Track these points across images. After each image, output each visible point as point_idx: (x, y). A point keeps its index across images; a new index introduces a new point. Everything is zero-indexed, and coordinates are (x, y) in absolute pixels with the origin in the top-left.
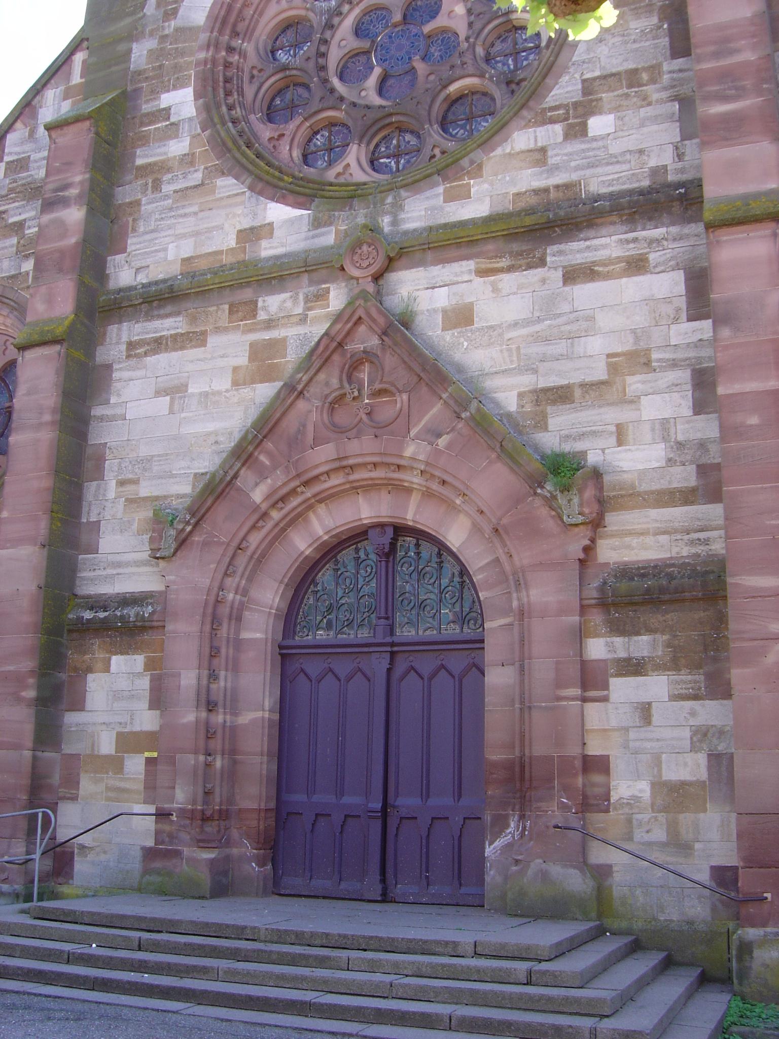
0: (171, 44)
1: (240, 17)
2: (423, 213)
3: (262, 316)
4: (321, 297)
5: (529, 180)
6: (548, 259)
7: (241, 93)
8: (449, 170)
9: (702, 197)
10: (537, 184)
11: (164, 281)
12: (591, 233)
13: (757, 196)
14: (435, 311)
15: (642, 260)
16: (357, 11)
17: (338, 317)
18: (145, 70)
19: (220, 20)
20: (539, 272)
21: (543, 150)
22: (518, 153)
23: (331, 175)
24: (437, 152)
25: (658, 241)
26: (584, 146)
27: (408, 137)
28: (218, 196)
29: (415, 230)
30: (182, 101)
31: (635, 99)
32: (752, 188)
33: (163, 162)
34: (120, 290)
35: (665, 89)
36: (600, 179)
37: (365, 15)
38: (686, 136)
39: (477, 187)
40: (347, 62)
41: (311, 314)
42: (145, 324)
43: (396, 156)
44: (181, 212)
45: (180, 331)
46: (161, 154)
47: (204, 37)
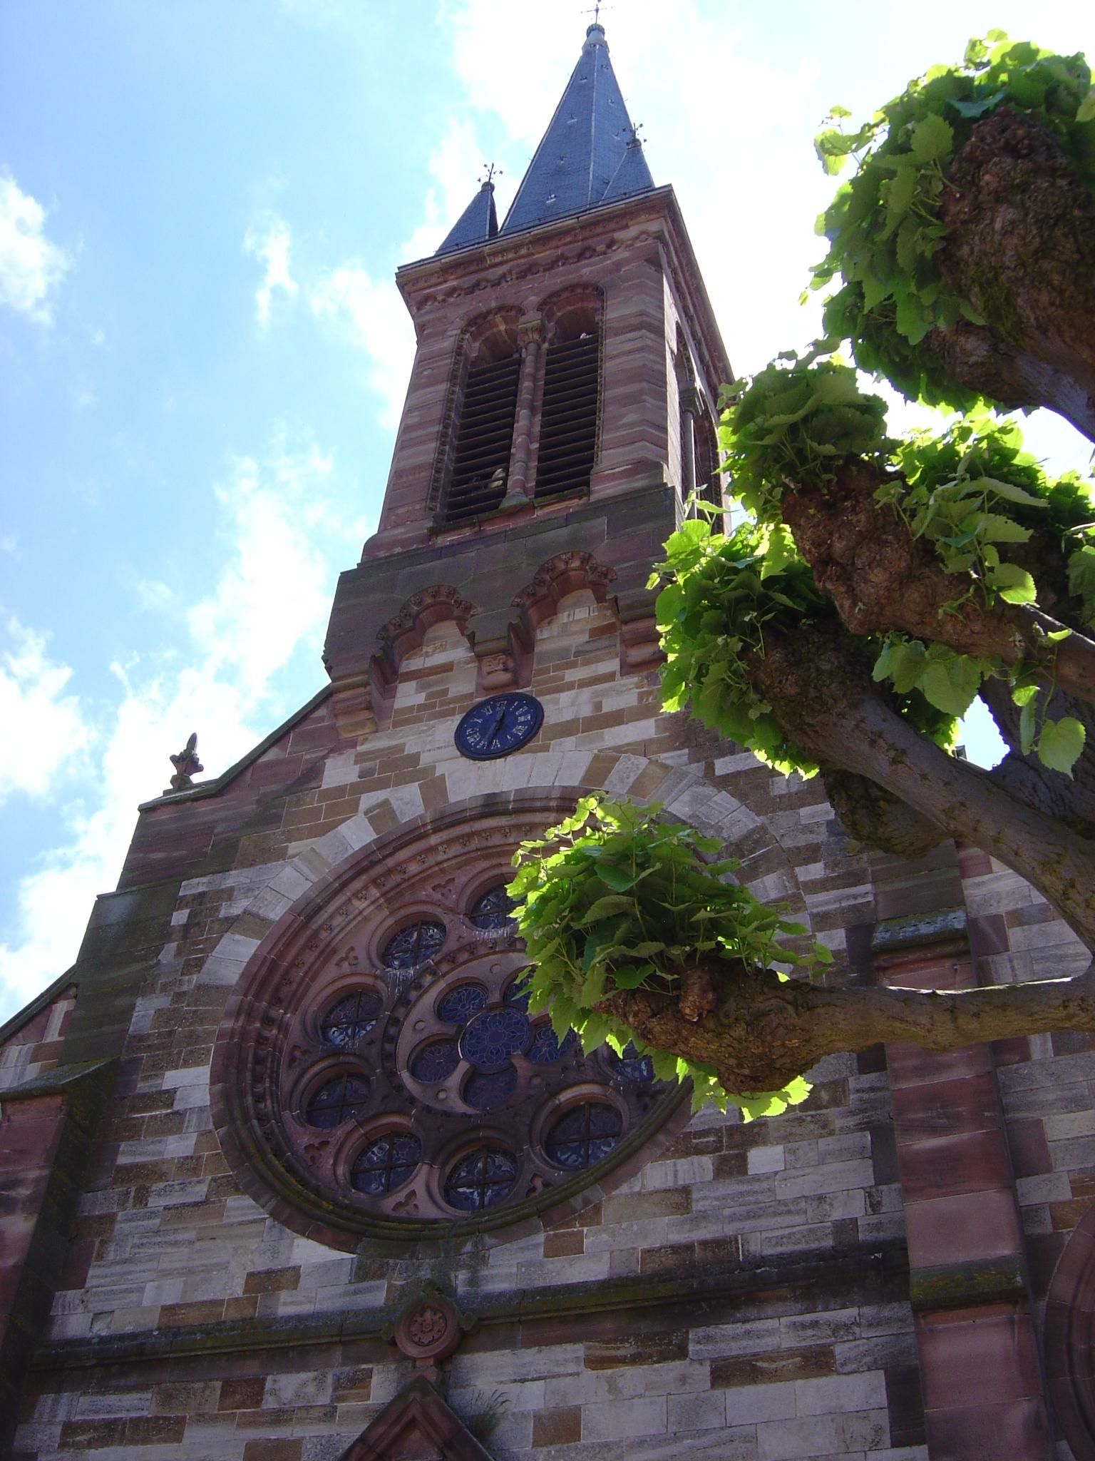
0: (188, 1005)
1: (286, 979)
2: (515, 1270)
3: (269, 1403)
4: (359, 1382)
5: (665, 1231)
6: (691, 1347)
7: (275, 1081)
8: (557, 1211)
9: (908, 1264)
10: (676, 1237)
11: (133, 1336)
12: (752, 1312)
13: (983, 1266)
14: (524, 1415)
15: (824, 1354)
16: (442, 985)
17: (381, 1416)
18: (149, 1035)
19: (258, 981)
20: (677, 1366)
21: (685, 1191)
22: (651, 1194)
23: (388, 1204)
24: (538, 1183)
25: (847, 1327)
26: (745, 1188)
27: (499, 1160)
28: (225, 1221)
29: (501, 1294)
30: (193, 1084)
31: (812, 1126)
32: (975, 1254)
33: (155, 1164)
34: (68, 1342)
35: (852, 1113)
36: (765, 1235)
37: (452, 991)
38: (882, 1178)
39: (592, 1238)
40: (423, 1051)
41: (342, 1406)
42: (95, 1398)
43: (481, 1185)
44: (171, 1238)
45: (145, 1413)
46: (153, 1154)
47: (234, 1000)
